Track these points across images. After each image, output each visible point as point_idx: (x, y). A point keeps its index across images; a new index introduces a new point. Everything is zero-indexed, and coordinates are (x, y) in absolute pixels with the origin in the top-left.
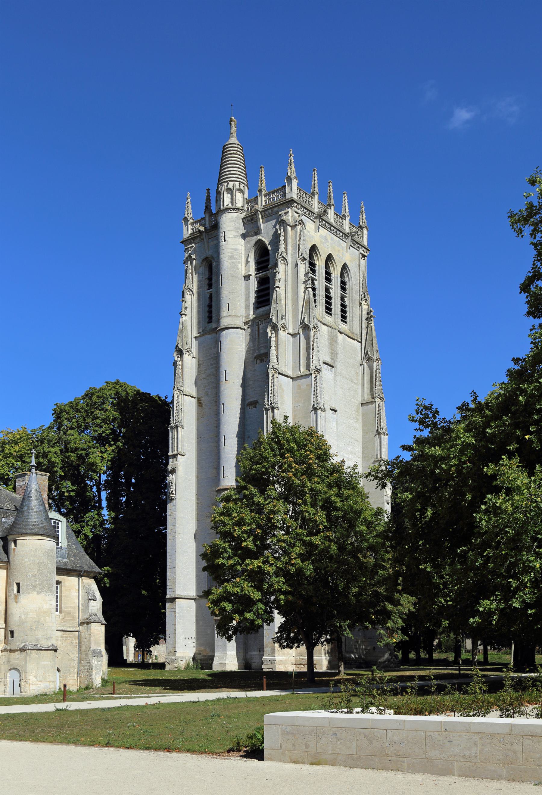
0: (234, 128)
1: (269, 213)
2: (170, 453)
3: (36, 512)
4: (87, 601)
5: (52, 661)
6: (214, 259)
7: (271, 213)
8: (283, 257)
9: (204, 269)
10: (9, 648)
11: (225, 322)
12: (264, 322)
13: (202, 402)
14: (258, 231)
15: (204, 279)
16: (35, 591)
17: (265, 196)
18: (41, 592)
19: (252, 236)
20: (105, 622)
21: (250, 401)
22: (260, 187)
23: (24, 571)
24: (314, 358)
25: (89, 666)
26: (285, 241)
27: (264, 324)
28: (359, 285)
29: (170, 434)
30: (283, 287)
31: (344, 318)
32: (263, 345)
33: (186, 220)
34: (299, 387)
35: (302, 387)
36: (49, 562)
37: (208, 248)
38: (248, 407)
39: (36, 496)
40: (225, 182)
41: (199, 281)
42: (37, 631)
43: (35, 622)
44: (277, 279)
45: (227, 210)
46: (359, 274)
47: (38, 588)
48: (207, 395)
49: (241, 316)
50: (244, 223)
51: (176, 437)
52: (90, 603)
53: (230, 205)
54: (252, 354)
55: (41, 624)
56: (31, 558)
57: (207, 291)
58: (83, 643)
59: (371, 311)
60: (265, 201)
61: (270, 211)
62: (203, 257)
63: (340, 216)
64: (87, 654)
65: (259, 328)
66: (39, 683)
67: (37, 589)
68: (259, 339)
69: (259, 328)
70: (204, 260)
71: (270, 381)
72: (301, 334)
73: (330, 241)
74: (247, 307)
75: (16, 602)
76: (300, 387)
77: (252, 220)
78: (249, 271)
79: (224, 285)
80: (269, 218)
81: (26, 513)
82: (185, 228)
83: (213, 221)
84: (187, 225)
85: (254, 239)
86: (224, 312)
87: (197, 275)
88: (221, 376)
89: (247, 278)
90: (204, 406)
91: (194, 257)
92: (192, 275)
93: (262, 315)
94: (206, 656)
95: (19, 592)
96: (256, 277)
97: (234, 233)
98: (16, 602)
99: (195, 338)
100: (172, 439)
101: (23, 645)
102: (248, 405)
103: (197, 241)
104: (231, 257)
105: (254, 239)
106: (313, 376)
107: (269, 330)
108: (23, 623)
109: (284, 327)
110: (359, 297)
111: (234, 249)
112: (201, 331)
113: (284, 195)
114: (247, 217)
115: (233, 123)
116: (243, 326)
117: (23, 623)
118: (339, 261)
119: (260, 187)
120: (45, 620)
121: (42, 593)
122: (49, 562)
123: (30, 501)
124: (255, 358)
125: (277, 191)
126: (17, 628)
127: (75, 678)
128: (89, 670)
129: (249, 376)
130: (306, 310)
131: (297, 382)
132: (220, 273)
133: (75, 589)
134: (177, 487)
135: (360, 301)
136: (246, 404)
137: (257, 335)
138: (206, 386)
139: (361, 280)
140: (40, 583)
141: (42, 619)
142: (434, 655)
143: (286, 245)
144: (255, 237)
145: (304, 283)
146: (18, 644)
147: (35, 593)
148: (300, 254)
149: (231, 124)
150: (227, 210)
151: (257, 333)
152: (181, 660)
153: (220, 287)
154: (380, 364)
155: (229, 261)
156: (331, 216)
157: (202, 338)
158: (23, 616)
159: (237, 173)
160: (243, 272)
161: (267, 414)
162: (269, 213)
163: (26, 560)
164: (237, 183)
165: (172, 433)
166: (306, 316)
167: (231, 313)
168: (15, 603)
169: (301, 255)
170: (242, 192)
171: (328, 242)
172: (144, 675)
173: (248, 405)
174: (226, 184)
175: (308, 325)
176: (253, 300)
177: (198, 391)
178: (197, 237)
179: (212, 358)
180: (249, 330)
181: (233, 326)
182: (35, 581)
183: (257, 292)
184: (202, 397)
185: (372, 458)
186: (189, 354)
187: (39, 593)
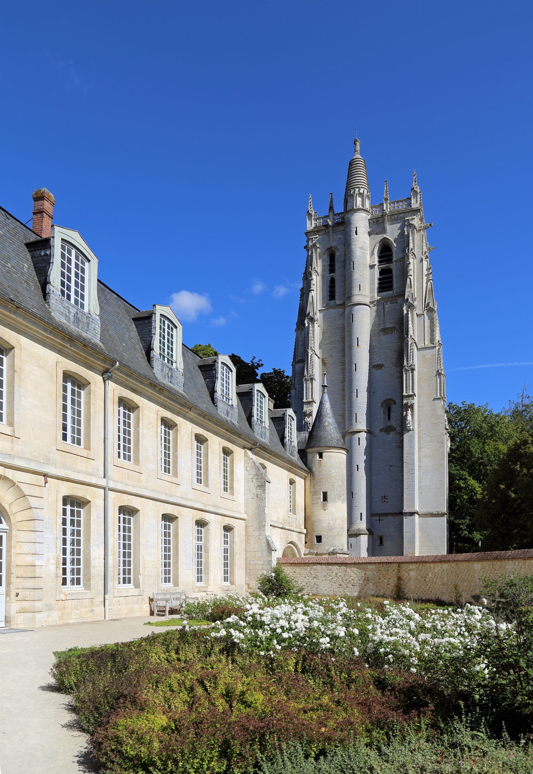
0: (358, 147)
1: (395, 218)
2: (305, 400)
8: (413, 253)
9: (326, 257)
10: (316, 552)
11: (356, 299)
12: (389, 303)
13: (326, 362)
14: (384, 231)
16: (340, 500)
17: (390, 204)
19: (377, 234)
21: (375, 364)
22: (385, 196)
23: (331, 481)
26: (413, 240)
27: (389, 305)
29: (305, 385)
33: (310, 215)
34: (424, 356)
38: (374, 369)
40: (356, 187)
41: (323, 266)
45: (359, 210)
48: (332, 357)
50: (369, 223)
51: (310, 387)
53: (361, 207)
54: (378, 327)
56: (337, 470)
60: (390, 208)
61: (396, 216)
62: (328, 246)
65: (384, 307)
68: (384, 316)
69: (384, 307)
70: (327, 249)
71: (309, 359)
72: (425, 315)
74: (372, 290)
75: (325, 510)
77: (377, 221)
78: (374, 262)
79: (355, 270)
80: (394, 222)
82: (308, 222)
84: (310, 219)
85: (380, 237)
86: (356, 291)
87: (321, 260)
88: (354, 342)
89: (372, 267)
90: (328, 366)
91: (318, 246)
92: (317, 260)
93: (388, 298)
96: (379, 268)
97: (364, 230)
98: (325, 510)
99: (319, 310)
100: (306, 389)
101: (332, 549)
102: (373, 367)
103: (321, 233)
104: (362, 248)
105: (380, 237)
106: (437, 348)
107: (306, 322)
108: (332, 529)
111: (364, 242)
112: (325, 305)
113: (410, 205)
114: (373, 219)
115: (358, 143)
116: (369, 303)
117: (332, 529)
119: (385, 196)
124: (380, 331)
125: (402, 201)
126: (326, 533)
129: (374, 344)
130: (429, 297)
131: (422, 352)
132: (351, 260)
138: (330, 350)
144: (380, 236)
145: (426, 275)
146: (327, 548)
147: (340, 502)
149: (355, 144)
150: (359, 210)
153: (351, 271)
154: (441, 349)
155: (361, 251)
157: (326, 311)
158: (331, 522)
160: (368, 262)
161: (406, 374)
162: (395, 218)
165: (306, 384)
166: (431, 301)
167: (361, 292)
168: (323, 510)
173: (373, 367)
174: (357, 190)
175: (432, 309)
176: (376, 286)
177: (323, 353)
178: (322, 230)
179: (336, 328)
180: (375, 308)
181: (364, 303)
182: (340, 491)
183: (379, 279)
184: (326, 358)
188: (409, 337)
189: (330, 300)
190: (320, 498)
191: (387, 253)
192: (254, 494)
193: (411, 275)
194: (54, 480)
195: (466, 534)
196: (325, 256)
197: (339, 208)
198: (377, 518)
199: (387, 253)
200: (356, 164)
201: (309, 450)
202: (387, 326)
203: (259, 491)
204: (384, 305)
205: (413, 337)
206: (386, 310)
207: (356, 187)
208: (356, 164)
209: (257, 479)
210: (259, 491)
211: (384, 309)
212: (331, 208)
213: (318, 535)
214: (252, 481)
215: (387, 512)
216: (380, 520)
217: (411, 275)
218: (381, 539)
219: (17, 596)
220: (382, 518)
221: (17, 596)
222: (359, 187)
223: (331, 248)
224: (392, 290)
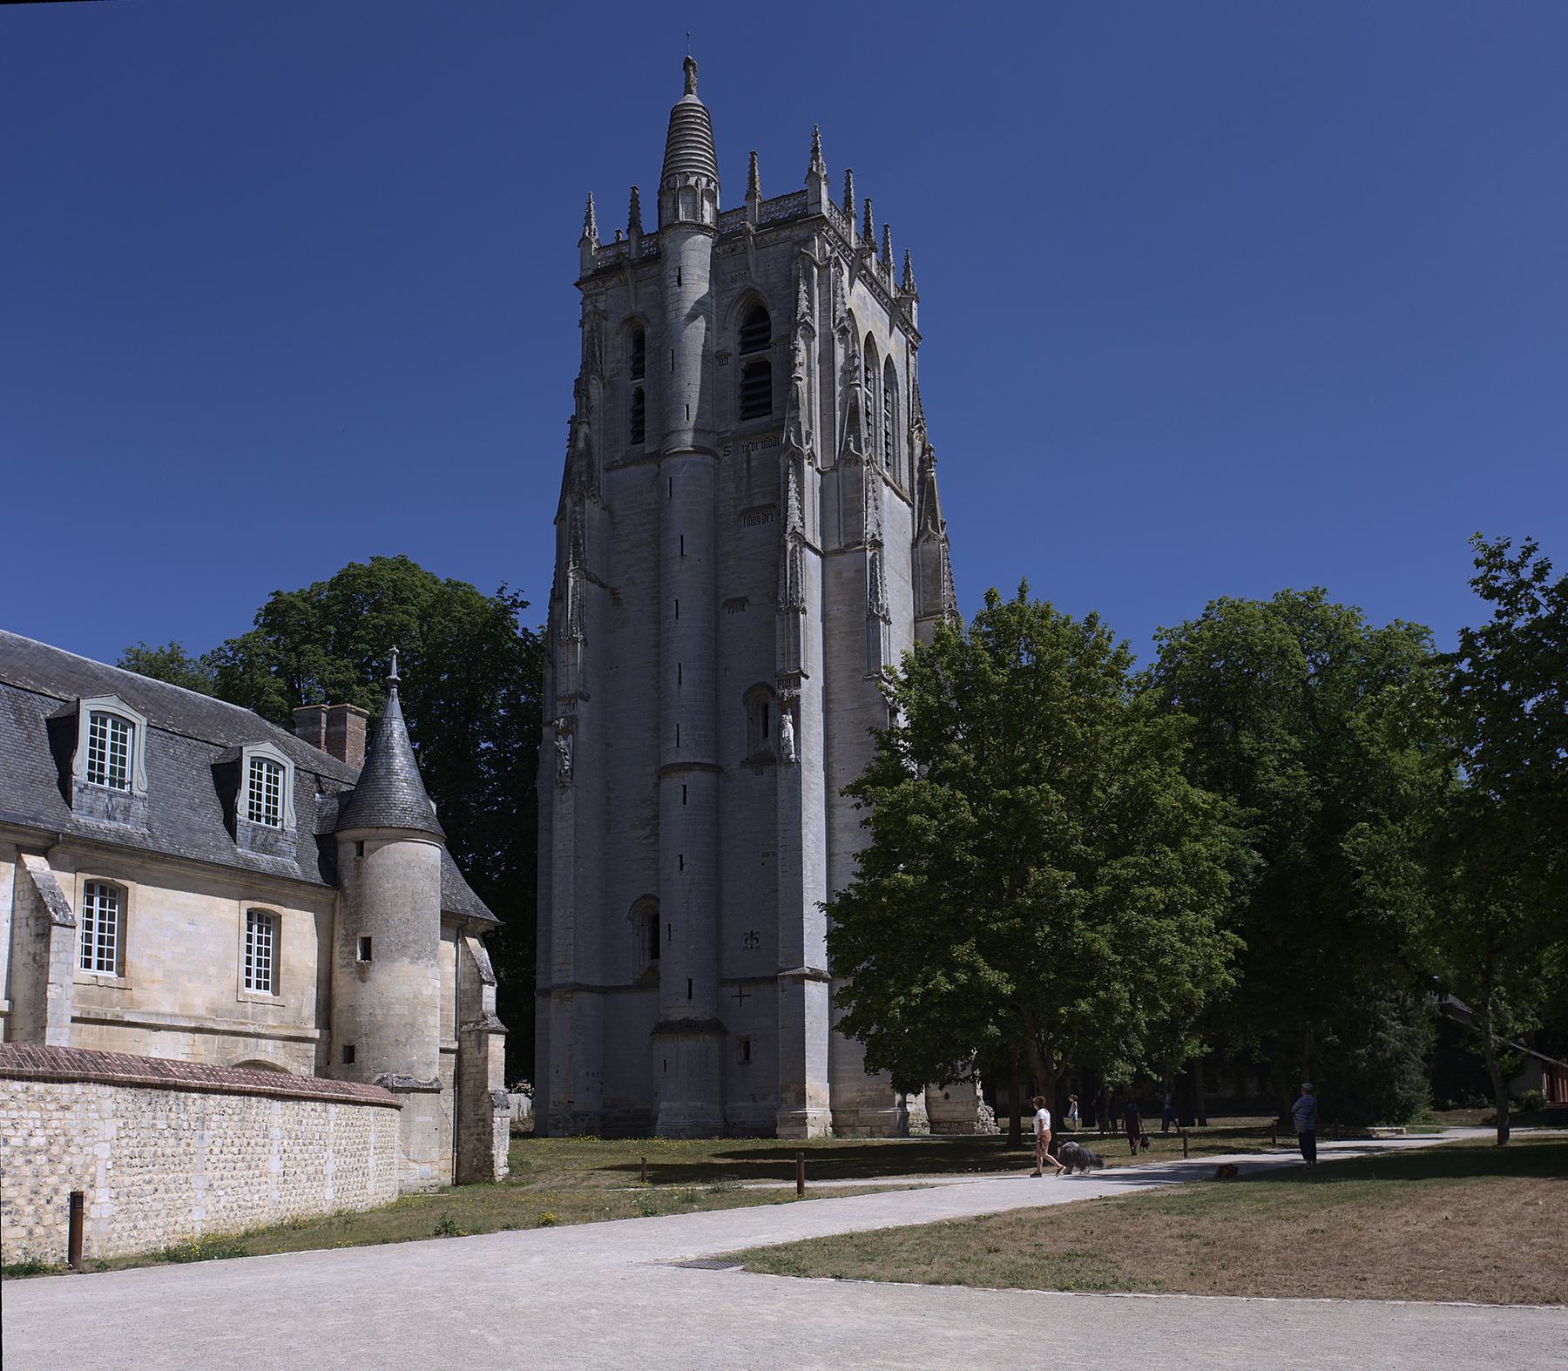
3: (406, 780)
4: (475, 986)
5: (436, 1115)
6: (648, 321)
7: (776, 240)
12: (759, 446)
13: (621, 596)
15: (624, 357)
16: (405, 955)
18: (418, 959)
20: (504, 1028)
24: (869, 519)
25: (484, 1127)
27: (760, 450)
28: (908, 398)
30: (805, 379)
31: (688, 419)
35: (844, 575)
36: (433, 893)
37: (636, 299)
39: (403, 746)
42: (408, 1047)
43: (405, 1026)
44: (797, 362)
46: (908, 376)
47: (412, 949)
49: (711, 431)
52: (484, 990)
55: (419, 1030)
57: (630, 383)
58: (465, 1078)
59: (931, 449)
63: (884, 265)
64: (478, 1100)
66: (412, 1165)
67: (411, 951)
69: (748, 456)
73: (870, 308)
75: (364, 982)
76: (841, 574)
77: (733, 250)
81: (383, 783)
83: (646, 248)
94: (629, 1111)
95: (367, 955)
98: (364, 982)
109: (812, 455)
110: (909, 422)
118: (883, 350)
120: (426, 1022)
121: (420, 961)
122: (433, 893)
123: (391, 757)
124: (741, 514)
127: (450, 1156)
128: (482, 1137)
133: (451, 958)
134: (575, 764)
135: (909, 429)
136: (721, 605)
137: (745, 471)
139: (911, 390)
140: (416, 938)
141: (421, 1019)
142: (1496, 1134)
143: (810, 300)
148: (837, 321)
151: (745, 466)
152: (582, 1120)
156: (872, 262)
159: (703, 159)
164: (704, 180)
169: (840, 323)
170: (713, 200)
171: (868, 309)
172: (684, 1152)
182: (407, 934)
186: (595, 500)
187: (415, 959)
188: (789, 530)
189: (634, 443)
190: (355, 953)
191: (760, 325)
192: (29, 954)
193: (800, 379)
194: (11, 906)
195: (1532, 1015)
196: (619, 337)
197: (649, 224)
198: (736, 991)
199: (760, 325)
200: (687, 117)
201: (341, 836)
202: (756, 504)
203: (40, 946)
204: (748, 451)
205: (799, 530)
206: (754, 463)
207: (679, 173)
208: (687, 117)
209: (37, 918)
210: (39, 946)
211: (749, 463)
212: (634, 223)
213: (346, 1043)
214: (27, 925)
215: (757, 975)
217: (800, 379)
218: (747, 1046)
219: (191, 1210)
220: (745, 991)
221: (191, 1210)
223: (632, 317)
224: (771, 413)
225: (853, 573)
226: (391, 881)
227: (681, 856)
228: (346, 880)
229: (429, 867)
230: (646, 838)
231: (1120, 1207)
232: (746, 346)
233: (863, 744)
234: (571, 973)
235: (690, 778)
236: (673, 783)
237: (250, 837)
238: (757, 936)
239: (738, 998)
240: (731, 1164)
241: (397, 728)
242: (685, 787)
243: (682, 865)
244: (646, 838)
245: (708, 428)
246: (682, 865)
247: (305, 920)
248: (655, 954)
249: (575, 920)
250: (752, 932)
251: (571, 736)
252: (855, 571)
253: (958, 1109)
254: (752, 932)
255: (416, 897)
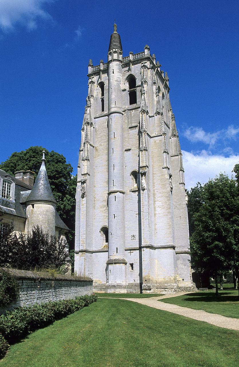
13: (98, 149)
32: (133, 121)
35: (156, 142)
76: (156, 141)
94: (100, 284)
163: (40, 217)
185: (178, 182)
206: (132, 115)
216: (131, 253)
220: (131, 251)
222: (114, 48)
225: (159, 141)
226: (42, 216)
227: (114, 215)
228: (29, 216)
229: (53, 212)
230: (105, 210)
231: (156, 310)
232: (130, 88)
233: (163, 184)
234: (85, 246)
235: (116, 194)
236: (113, 195)
237: (2, 202)
238: (135, 236)
239: (131, 253)
240: (193, 298)
241: (89, 93)
242: (115, 196)
243: (115, 217)
244: (105, 210)
245: (121, 107)
246: (115, 217)
247: (17, 227)
248: (107, 241)
249: (86, 231)
250: (133, 235)
251: (85, 184)
252: (159, 141)
253: (186, 283)
254: (133, 235)
255: (49, 220)
